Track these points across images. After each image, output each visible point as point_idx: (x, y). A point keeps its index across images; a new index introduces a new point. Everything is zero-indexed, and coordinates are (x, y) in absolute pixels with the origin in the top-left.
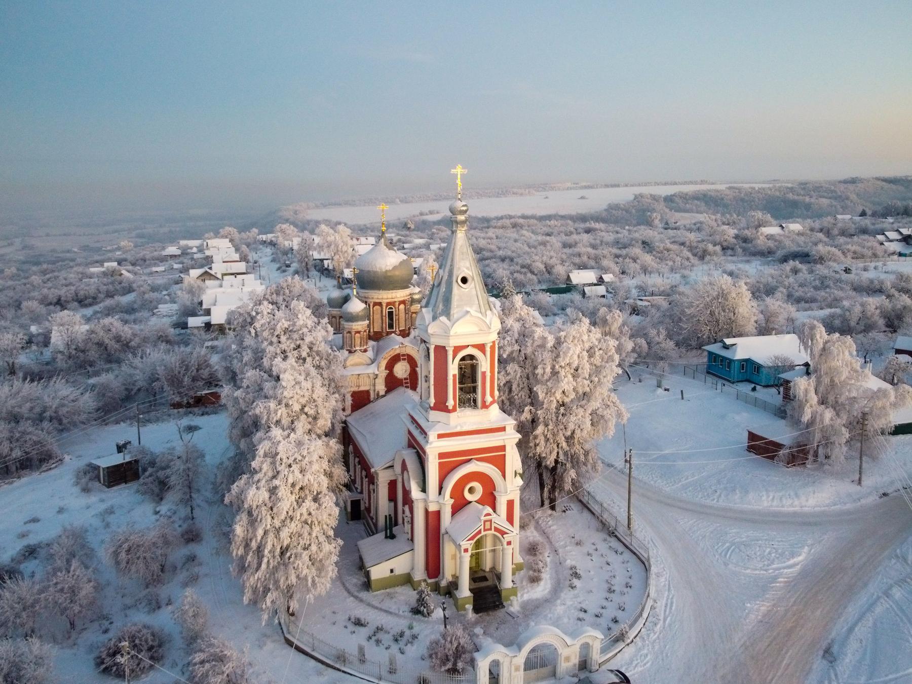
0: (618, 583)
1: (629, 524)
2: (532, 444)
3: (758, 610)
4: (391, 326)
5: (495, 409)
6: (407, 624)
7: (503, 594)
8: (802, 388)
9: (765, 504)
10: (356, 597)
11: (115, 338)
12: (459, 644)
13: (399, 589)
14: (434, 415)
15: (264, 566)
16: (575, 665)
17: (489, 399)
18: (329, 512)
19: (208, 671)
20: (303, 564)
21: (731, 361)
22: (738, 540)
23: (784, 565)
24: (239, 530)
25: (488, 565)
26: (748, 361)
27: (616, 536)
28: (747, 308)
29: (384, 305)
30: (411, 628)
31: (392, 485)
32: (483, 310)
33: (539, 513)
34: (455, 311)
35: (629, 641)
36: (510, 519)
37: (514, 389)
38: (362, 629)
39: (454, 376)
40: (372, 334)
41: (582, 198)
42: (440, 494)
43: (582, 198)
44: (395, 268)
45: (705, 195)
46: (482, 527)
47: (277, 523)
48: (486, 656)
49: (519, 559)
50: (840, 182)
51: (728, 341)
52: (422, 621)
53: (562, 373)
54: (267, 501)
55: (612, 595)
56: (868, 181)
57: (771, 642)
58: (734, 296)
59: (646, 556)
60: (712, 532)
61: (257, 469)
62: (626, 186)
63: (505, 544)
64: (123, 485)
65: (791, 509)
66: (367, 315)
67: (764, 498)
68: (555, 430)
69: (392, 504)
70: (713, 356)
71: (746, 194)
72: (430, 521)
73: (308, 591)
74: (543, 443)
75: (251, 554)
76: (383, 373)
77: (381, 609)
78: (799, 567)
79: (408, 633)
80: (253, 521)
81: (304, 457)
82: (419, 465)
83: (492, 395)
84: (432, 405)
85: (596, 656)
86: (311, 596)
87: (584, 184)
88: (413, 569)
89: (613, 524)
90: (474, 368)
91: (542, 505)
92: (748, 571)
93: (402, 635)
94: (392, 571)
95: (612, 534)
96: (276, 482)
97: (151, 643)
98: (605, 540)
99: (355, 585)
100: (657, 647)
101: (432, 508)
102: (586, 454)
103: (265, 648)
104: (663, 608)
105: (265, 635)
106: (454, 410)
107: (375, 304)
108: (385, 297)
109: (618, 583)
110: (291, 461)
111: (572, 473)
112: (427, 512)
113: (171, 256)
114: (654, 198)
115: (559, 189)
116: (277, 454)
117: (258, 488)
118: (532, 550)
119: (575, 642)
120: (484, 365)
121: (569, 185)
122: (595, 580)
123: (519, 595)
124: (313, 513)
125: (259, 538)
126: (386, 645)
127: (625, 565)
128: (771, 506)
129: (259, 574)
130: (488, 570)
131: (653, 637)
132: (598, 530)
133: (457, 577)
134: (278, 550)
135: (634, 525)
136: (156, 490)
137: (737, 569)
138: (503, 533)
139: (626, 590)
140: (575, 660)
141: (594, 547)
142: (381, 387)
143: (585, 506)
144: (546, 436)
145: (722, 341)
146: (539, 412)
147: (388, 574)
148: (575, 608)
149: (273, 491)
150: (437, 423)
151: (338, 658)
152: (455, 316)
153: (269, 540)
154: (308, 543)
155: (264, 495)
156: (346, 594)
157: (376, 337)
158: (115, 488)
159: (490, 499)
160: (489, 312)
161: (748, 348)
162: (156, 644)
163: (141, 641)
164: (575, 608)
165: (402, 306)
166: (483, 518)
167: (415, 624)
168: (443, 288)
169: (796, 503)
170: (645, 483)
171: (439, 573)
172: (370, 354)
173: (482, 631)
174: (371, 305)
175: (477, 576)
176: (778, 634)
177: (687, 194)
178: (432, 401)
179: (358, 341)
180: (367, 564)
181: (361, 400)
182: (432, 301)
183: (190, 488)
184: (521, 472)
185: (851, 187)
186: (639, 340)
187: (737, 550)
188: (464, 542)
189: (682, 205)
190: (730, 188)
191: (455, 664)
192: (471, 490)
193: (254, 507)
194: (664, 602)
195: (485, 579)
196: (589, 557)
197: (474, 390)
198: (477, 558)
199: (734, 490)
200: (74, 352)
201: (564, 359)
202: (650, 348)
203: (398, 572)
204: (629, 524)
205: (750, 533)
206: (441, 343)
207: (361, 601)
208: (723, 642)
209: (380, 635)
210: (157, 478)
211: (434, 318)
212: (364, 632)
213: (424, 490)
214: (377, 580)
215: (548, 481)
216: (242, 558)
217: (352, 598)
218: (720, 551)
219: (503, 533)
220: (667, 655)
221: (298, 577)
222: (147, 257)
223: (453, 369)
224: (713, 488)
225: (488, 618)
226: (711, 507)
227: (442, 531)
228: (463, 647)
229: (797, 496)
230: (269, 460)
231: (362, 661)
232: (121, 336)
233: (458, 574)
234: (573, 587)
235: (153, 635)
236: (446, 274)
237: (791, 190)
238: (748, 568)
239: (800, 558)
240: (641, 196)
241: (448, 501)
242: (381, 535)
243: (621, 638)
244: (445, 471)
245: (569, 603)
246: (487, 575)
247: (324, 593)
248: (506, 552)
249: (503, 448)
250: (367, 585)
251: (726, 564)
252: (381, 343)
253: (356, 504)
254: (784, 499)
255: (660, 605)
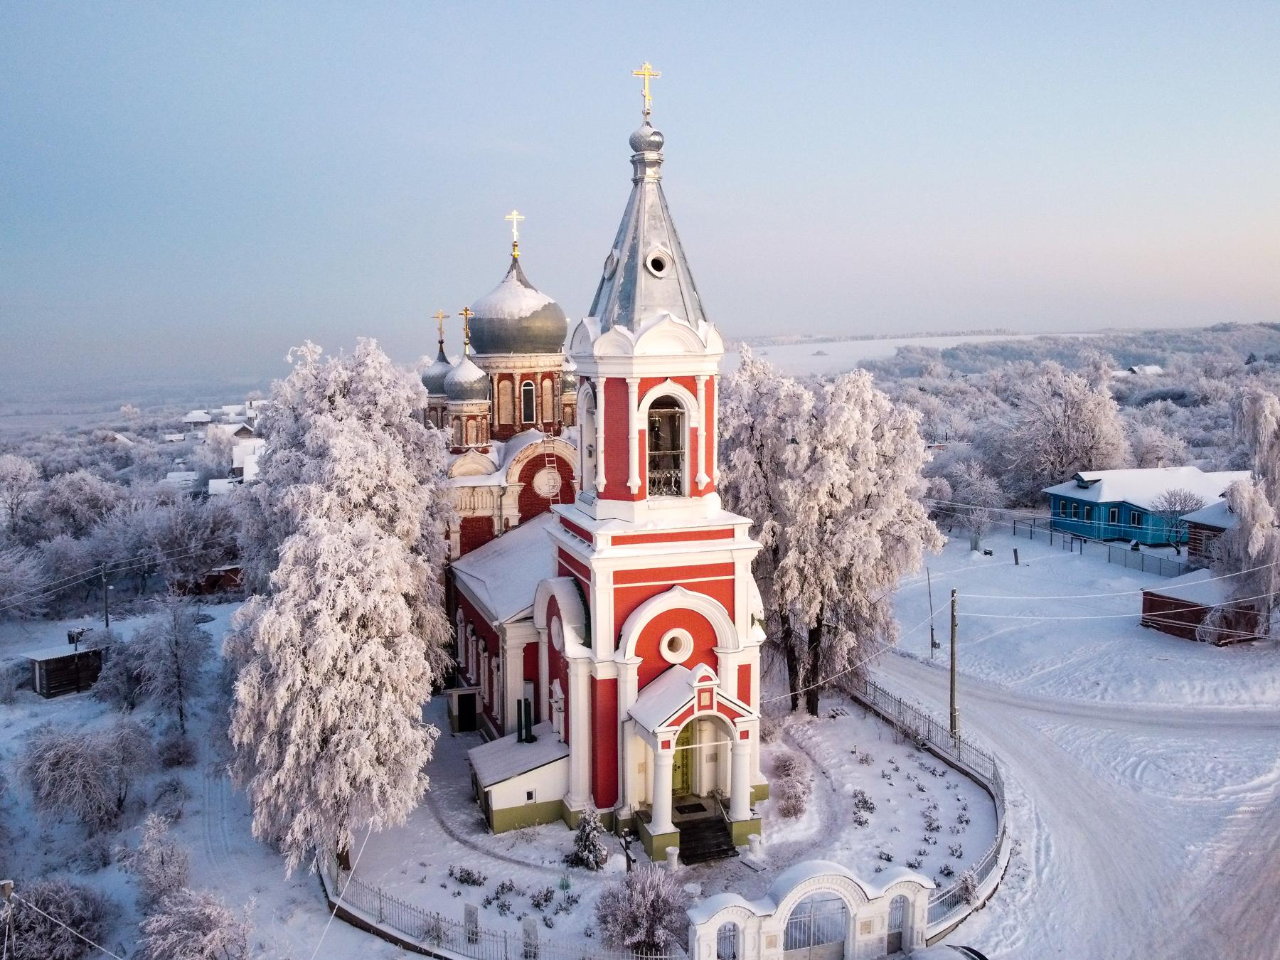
0: (945, 816)
1: (953, 726)
2: (777, 587)
3: (1211, 856)
4: (529, 416)
5: (714, 500)
6: (559, 881)
7: (735, 831)
8: (1246, 495)
9: (1189, 700)
10: (464, 842)
11: (88, 501)
12: (658, 896)
13: (543, 829)
14: (606, 507)
15: (289, 760)
16: (881, 940)
17: (703, 479)
18: (413, 668)
19: (172, 947)
20: (362, 757)
21: (1093, 506)
22: (1151, 751)
23: (1244, 786)
24: (243, 691)
25: (704, 786)
26: (1122, 506)
27: (929, 750)
28: (1111, 423)
29: (517, 379)
30: (565, 886)
31: (531, 652)
32: (691, 317)
33: (789, 720)
34: (643, 318)
35: (978, 903)
36: (744, 694)
37: (742, 495)
38: (474, 890)
39: (641, 433)
40: (496, 428)
41: (819, 353)
42: (617, 647)
43: (819, 353)
44: (535, 315)
45: (1003, 349)
46: (695, 701)
47: (316, 681)
48: (712, 915)
49: (763, 780)
50: (1206, 330)
51: (1087, 476)
52: (588, 877)
53: (831, 456)
54: (297, 639)
55: (934, 834)
56: (1248, 327)
57: (1249, 905)
58: (1092, 406)
59: (989, 775)
60: (1102, 742)
61: (280, 583)
62: (884, 337)
63: (738, 735)
64: (74, 695)
65: (1237, 707)
66: (488, 390)
67: (1186, 690)
68: (818, 560)
69: (531, 686)
70: (1061, 504)
71: (1065, 347)
72: (599, 697)
73: (373, 810)
74: (796, 583)
75: (266, 739)
76: (515, 488)
77: (510, 860)
78: (1272, 789)
79: (559, 895)
80: (269, 678)
81: (366, 564)
82: (582, 607)
83: (709, 471)
84: (601, 489)
85: (921, 925)
86: (378, 819)
87: (819, 337)
88: (568, 792)
89: (923, 732)
90: (674, 423)
91: (794, 706)
92: (1179, 798)
93: (548, 897)
94: (530, 796)
95: (922, 746)
96: (315, 604)
97: (78, 912)
98: (911, 756)
99: (464, 824)
100: (1031, 915)
101: (604, 674)
102: (873, 607)
103: (290, 922)
104: (1033, 853)
105: (294, 901)
106: (641, 496)
107: (503, 377)
108: (519, 364)
109: (945, 816)
110: (341, 571)
111: (849, 639)
112: (593, 682)
113: (196, 424)
114: (929, 353)
115: (783, 344)
116: (317, 557)
117: (279, 613)
118: (782, 768)
119: (882, 893)
120: (694, 415)
121: (798, 337)
122: (901, 812)
123: (763, 835)
124: (383, 666)
125: (281, 706)
126: (517, 914)
127: (952, 791)
128: (1201, 703)
129: (281, 775)
130: (704, 794)
131: (1022, 899)
132: (896, 742)
133: (650, 806)
134: (317, 731)
135: (963, 730)
136: (123, 689)
137: (1158, 795)
138: (734, 715)
139: (960, 827)
140: (881, 931)
141: (894, 766)
142: (512, 511)
143: (866, 708)
144: (801, 571)
145: (1076, 477)
146: (789, 529)
147: (523, 801)
148: (869, 855)
149: (308, 621)
150: (609, 519)
151: (427, 932)
152: (643, 324)
153: (299, 710)
154: (373, 720)
155: (289, 624)
156: (445, 836)
157: (504, 434)
158: (61, 698)
159: (708, 653)
160: (701, 322)
161: (1117, 485)
162: (88, 914)
163: (59, 907)
164: (869, 855)
165: (547, 383)
166: (697, 685)
167: (572, 881)
168: (620, 278)
169: (1245, 696)
170: (970, 677)
171: (616, 798)
172: (493, 455)
173: (699, 890)
174: (496, 379)
175: (684, 803)
176: (1259, 893)
177: (976, 347)
178: (602, 482)
179: (472, 434)
180: (485, 779)
181: (477, 534)
182: (601, 308)
183: (179, 677)
184: (762, 617)
185: (1223, 336)
186: (937, 480)
187: (1152, 766)
188: (663, 728)
189: (969, 363)
190: (1041, 339)
191: (651, 932)
192: (673, 645)
193: (273, 648)
194: (1033, 844)
195: (699, 808)
196: (886, 780)
197: (676, 462)
198: (685, 766)
199: (1129, 680)
200: (21, 522)
201: (832, 429)
202: (954, 487)
203: (540, 798)
204: (953, 726)
205: (1171, 741)
206: (615, 371)
207: (474, 847)
208: (1156, 907)
209: (508, 898)
210: (127, 670)
211: (605, 330)
212: (475, 896)
213: (588, 643)
214: (502, 811)
215: (808, 664)
216: (251, 750)
217: (457, 843)
218: (1120, 770)
219: (734, 715)
220: (1053, 928)
221: (353, 782)
222: (159, 425)
223: (639, 420)
224: (1092, 679)
225: (708, 871)
226: (1092, 708)
227: (622, 716)
228: (665, 902)
229: (1244, 685)
230: (302, 569)
231: (473, 938)
232: (98, 499)
233: (650, 801)
234: (861, 823)
235: (85, 899)
236: (626, 253)
237: (1133, 340)
238: (1178, 793)
239: (1272, 776)
240: (908, 349)
241: (631, 663)
242: (511, 739)
243: (964, 895)
244: (626, 608)
245: (857, 847)
246: (702, 802)
247: (402, 820)
248: (740, 751)
249: (729, 568)
250: (486, 823)
251: (1136, 789)
252: (511, 442)
253: (467, 702)
254: (1221, 692)
255: (1028, 848)
